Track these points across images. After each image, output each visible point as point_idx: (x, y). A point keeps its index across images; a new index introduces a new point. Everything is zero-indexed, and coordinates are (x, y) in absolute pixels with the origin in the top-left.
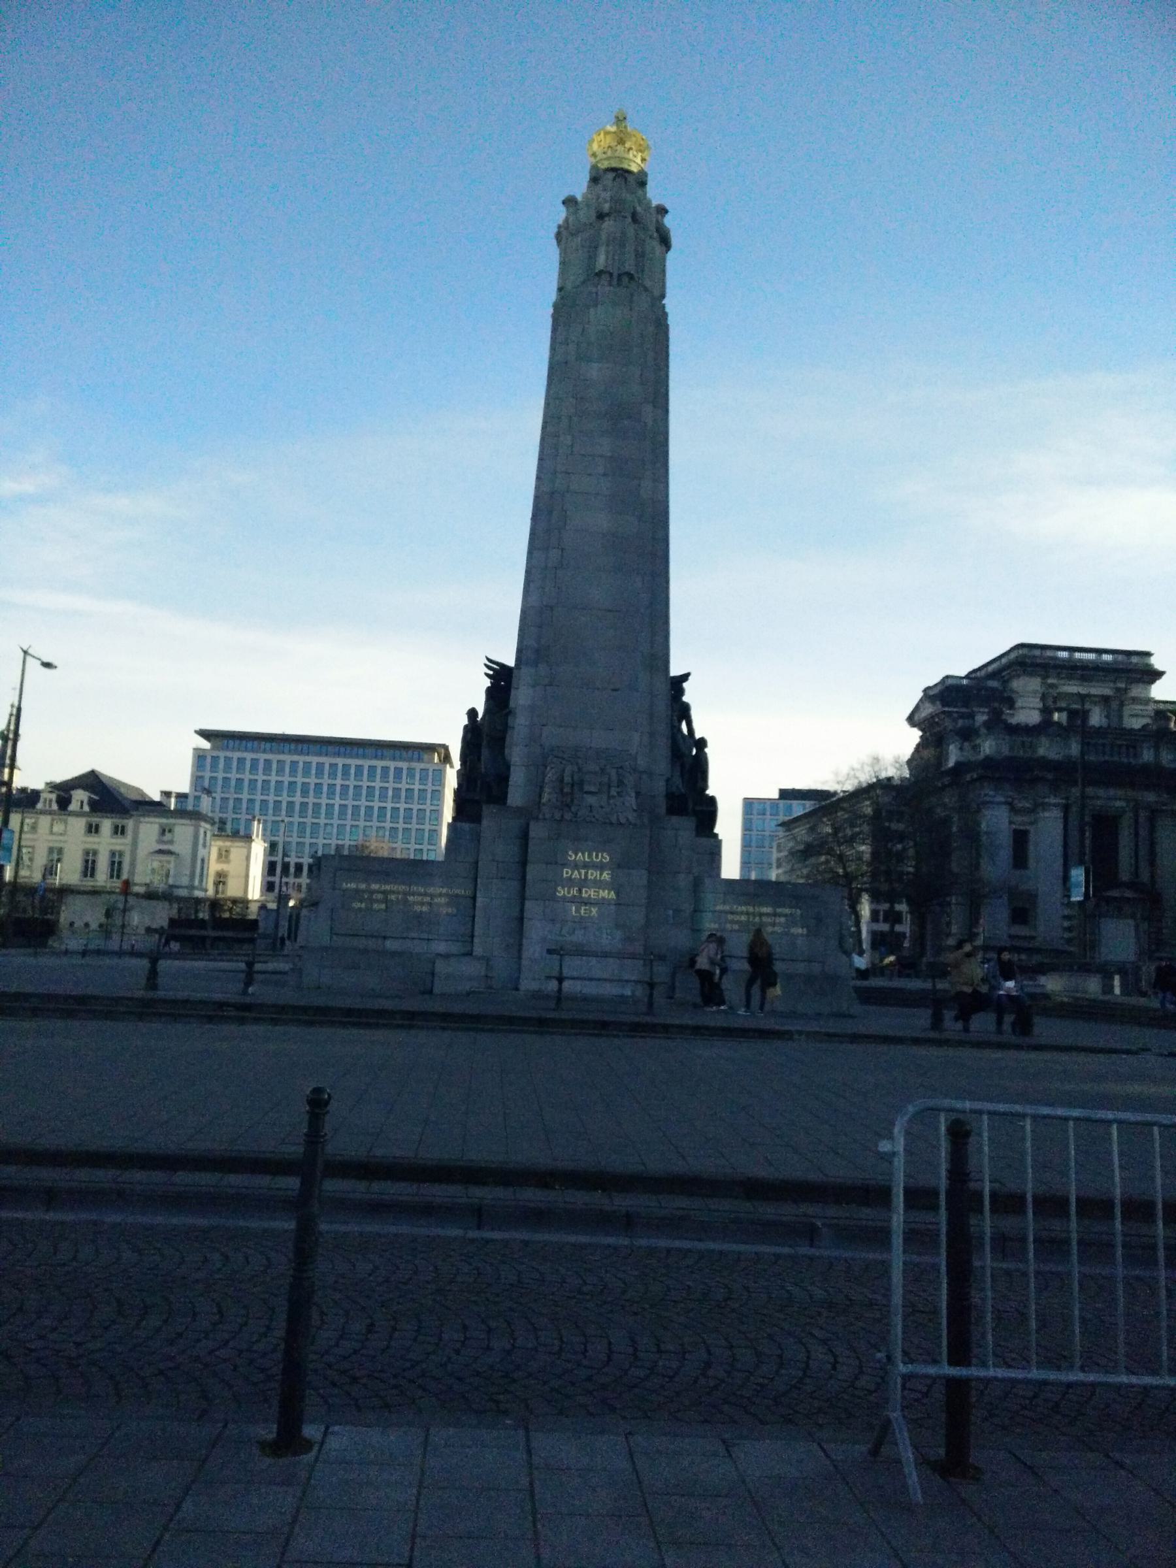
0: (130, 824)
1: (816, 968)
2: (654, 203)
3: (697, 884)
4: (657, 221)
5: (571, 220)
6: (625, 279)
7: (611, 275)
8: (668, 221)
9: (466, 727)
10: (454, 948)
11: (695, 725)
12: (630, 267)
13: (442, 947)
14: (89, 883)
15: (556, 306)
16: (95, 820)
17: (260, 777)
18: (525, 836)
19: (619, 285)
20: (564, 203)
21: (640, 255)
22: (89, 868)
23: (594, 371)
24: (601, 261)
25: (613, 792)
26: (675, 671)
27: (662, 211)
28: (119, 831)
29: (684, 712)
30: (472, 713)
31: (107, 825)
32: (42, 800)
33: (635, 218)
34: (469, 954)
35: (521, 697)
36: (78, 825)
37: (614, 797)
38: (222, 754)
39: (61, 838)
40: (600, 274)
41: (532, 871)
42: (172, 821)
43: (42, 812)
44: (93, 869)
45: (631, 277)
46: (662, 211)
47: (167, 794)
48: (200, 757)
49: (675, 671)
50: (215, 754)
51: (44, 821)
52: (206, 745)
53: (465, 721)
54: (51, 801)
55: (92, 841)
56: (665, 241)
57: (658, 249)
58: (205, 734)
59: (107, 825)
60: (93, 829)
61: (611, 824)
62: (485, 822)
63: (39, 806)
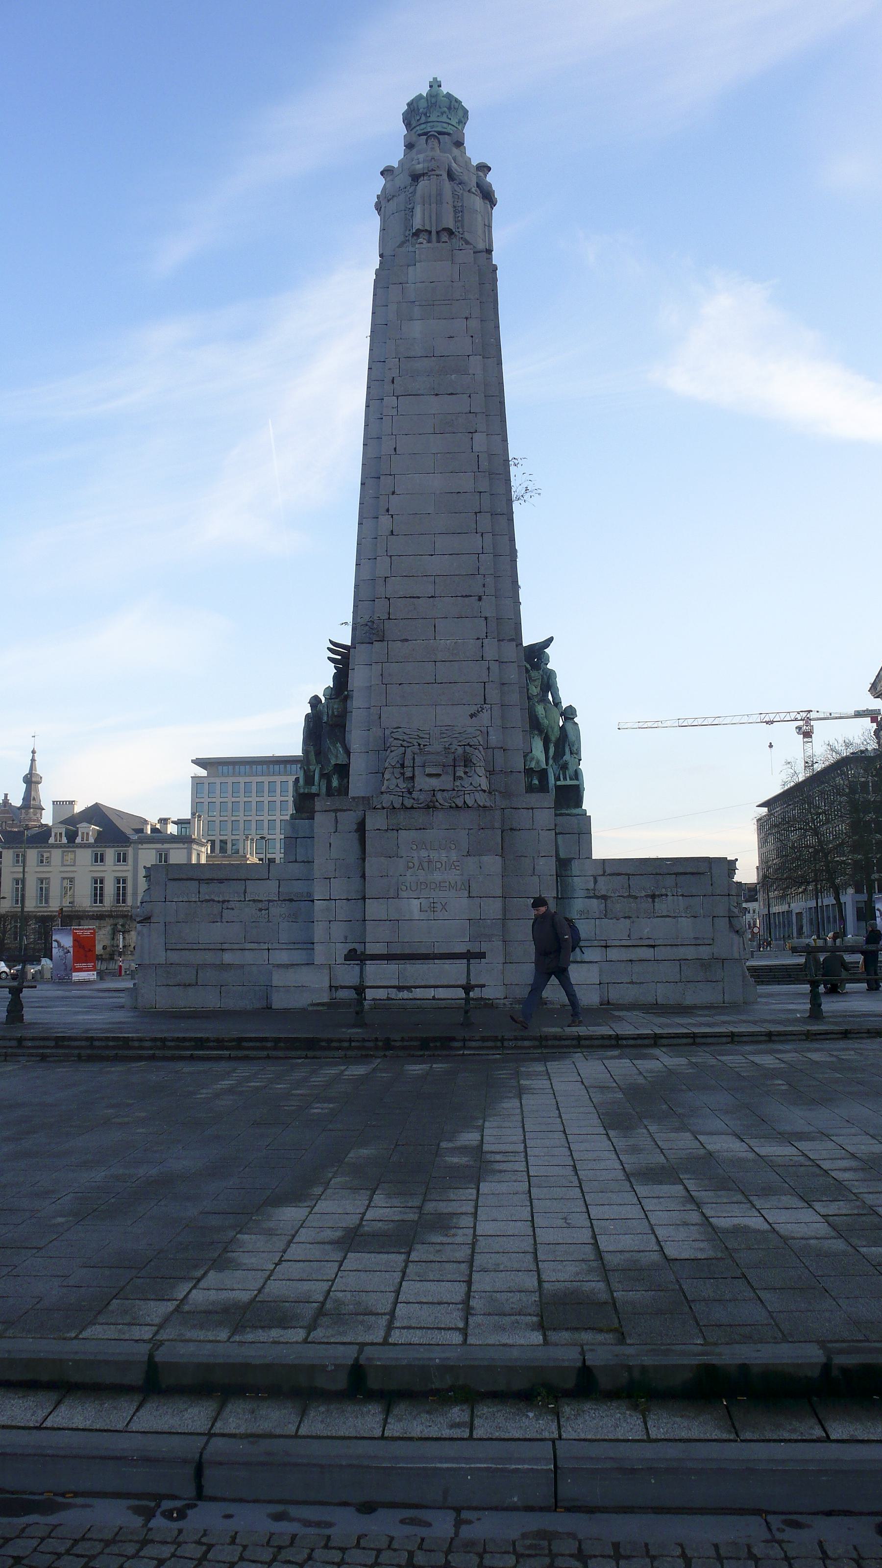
0: (130, 851)
1: (704, 952)
2: (474, 163)
3: (563, 865)
4: (478, 177)
5: (387, 186)
6: (445, 237)
7: (430, 232)
8: (490, 178)
9: (307, 716)
10: (298, 957)
11: (562, 694)
12: (449, 222)
13: (282, 957)
14: (98, 908)
15: (378, 273)
16: (99, 850)
17: (254, 799)
18: (361, 828)
19: (438, 242)
20: (382, 173)
21: (459, 211)
22: (98, 894)
23: (416, 329)
24: (417, 223)
25: (460, 773)
26: (528, 639)
27: (484, 168)
28: (122, 858)
29: (548, 683)
30: (315, 702)
31: (110, 854)
32: (53, 834)
33: (451, 176)
34: (310, 964)
35: (357, 679)
36: (85, 856)
37: (461, 778)
38: (218, 780)
39: (72, 869)
40: (417, 234)
41: (372, 865)
42: (166, 846)
43: (53, 846)
44: (101, 895)
45: (450, 232)
46: (484, 168)
47: (164, 821)
48: (197, 782)
49: (528, 639)
50: (212, 780)
51: (56, 854)
52: (203, 773)
53: (308, 710)
54: (61, 834)
55: (99, 870)
56: (488, 197)
57: (478, 202)
58: (331, 642)
59: (110, 854)
60: (99, 858)
61: (457, 807)
62: (318, 817)
63: (52, 840)
